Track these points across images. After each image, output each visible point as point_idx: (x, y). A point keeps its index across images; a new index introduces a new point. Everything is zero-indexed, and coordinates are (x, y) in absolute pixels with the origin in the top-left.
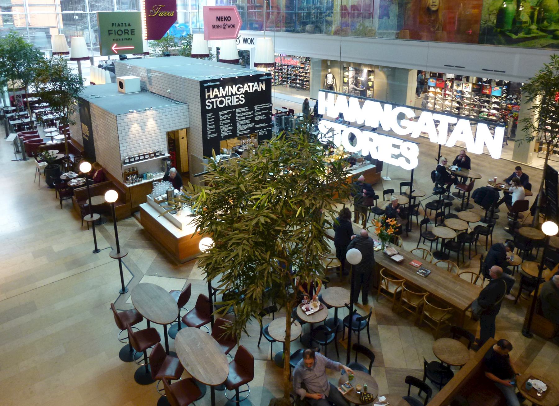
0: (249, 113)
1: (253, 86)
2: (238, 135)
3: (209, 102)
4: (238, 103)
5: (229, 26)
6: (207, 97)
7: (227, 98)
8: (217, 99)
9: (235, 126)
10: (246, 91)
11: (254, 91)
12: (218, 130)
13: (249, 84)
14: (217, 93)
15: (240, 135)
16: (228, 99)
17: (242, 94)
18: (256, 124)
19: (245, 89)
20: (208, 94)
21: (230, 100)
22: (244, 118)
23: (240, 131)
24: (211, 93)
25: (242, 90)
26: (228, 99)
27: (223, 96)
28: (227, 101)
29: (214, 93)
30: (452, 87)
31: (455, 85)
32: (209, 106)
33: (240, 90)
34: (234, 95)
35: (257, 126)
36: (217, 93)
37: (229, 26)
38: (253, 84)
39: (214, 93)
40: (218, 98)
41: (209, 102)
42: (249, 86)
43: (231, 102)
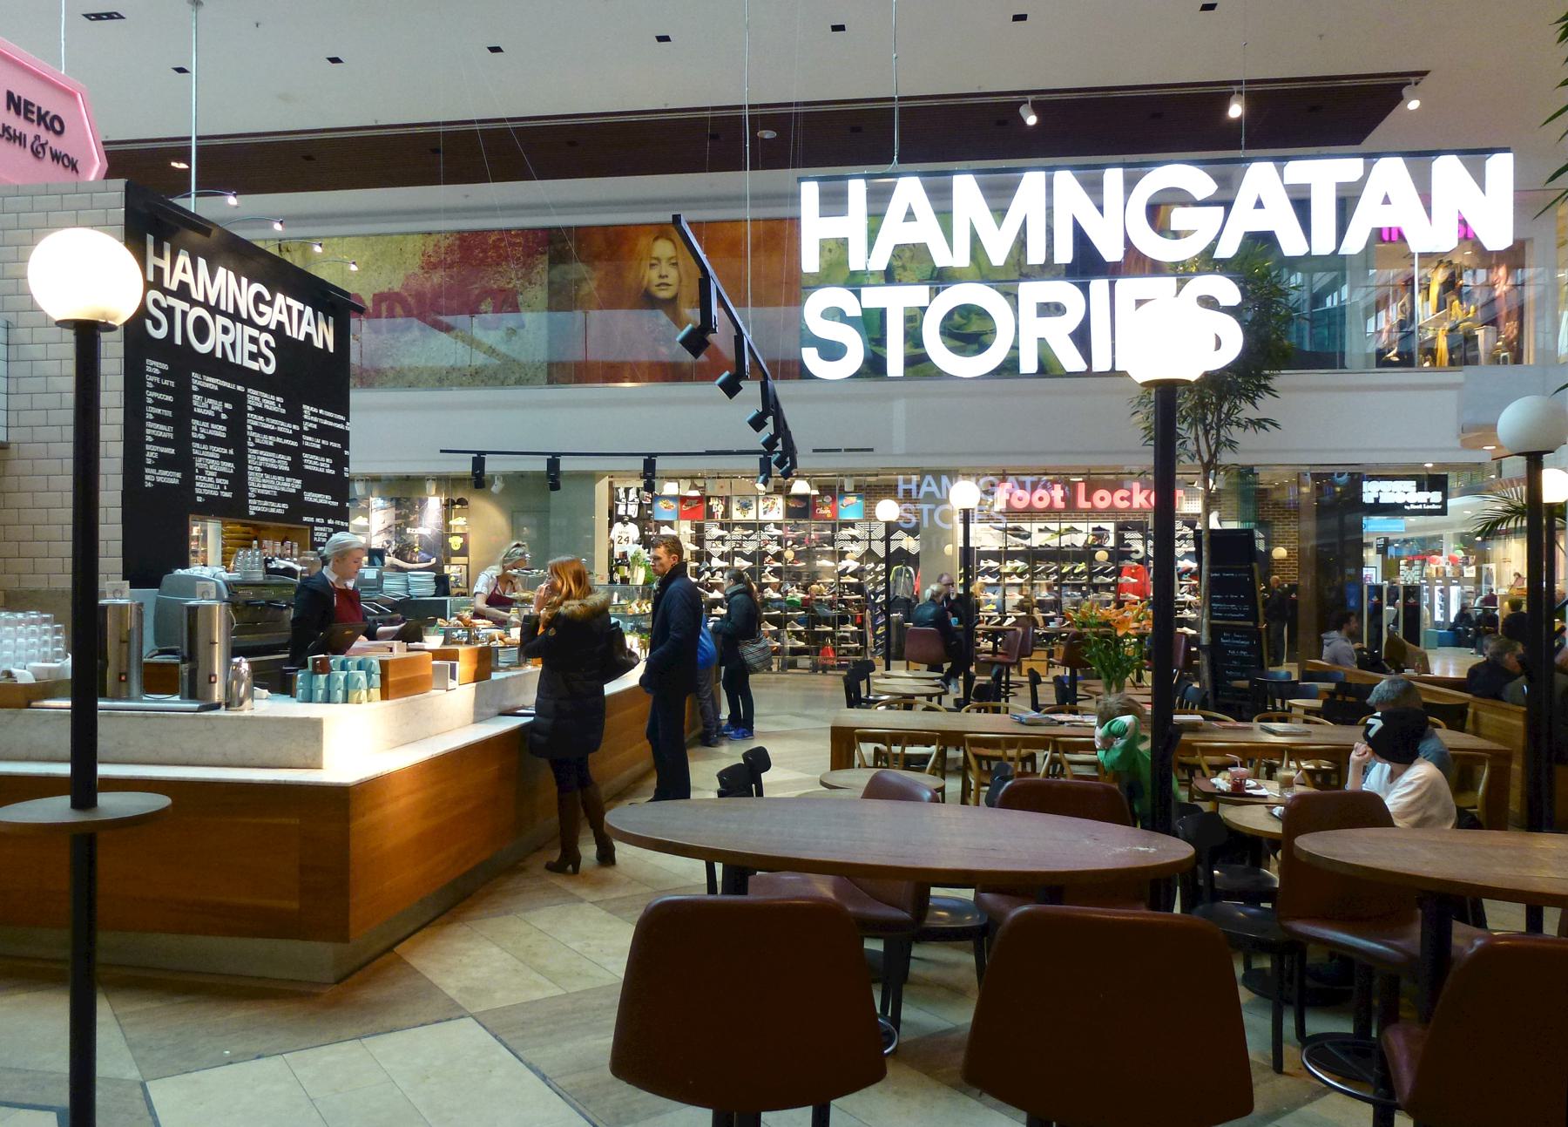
0: (286, 427)
1: (1346, 204)
2: (252, 511)
3: (836, 314)
4: (254, 366)
5: (56, 157)
6: (810, 262)
7: (1032, 292)
8: (916, 295)
9: (240, 461)
10: (1261, 242)
11: (1354, 243)
12: (183, 461)
13: (1301, 170)
14: (926, 230)
15: (259, 515)
16: (1050, 309)
17: (1208, 262)
18: (307, 486)
19: (1245, 220)
20: (834, 227)
21: (1072, 320)
22: (270, 441)
23: (259, 497)
24: (852, 225)
25: (271, 317)
26: (1050, 309)
27: (980, 270)
28: (1034, 328)
29: (895, 231)
30: (727, 513)
31: (735, 506)
32: (832, 351)
33: (1179, 218)
34: (1112, 271)
35: (310, 497)
36: (926, 230)
37: (56, 157)
38: (1348, 168)
39: (895, 231)
40: (940, 279)
41: (836, 314)
42: (1302, 205)
43: (1082, 337)
